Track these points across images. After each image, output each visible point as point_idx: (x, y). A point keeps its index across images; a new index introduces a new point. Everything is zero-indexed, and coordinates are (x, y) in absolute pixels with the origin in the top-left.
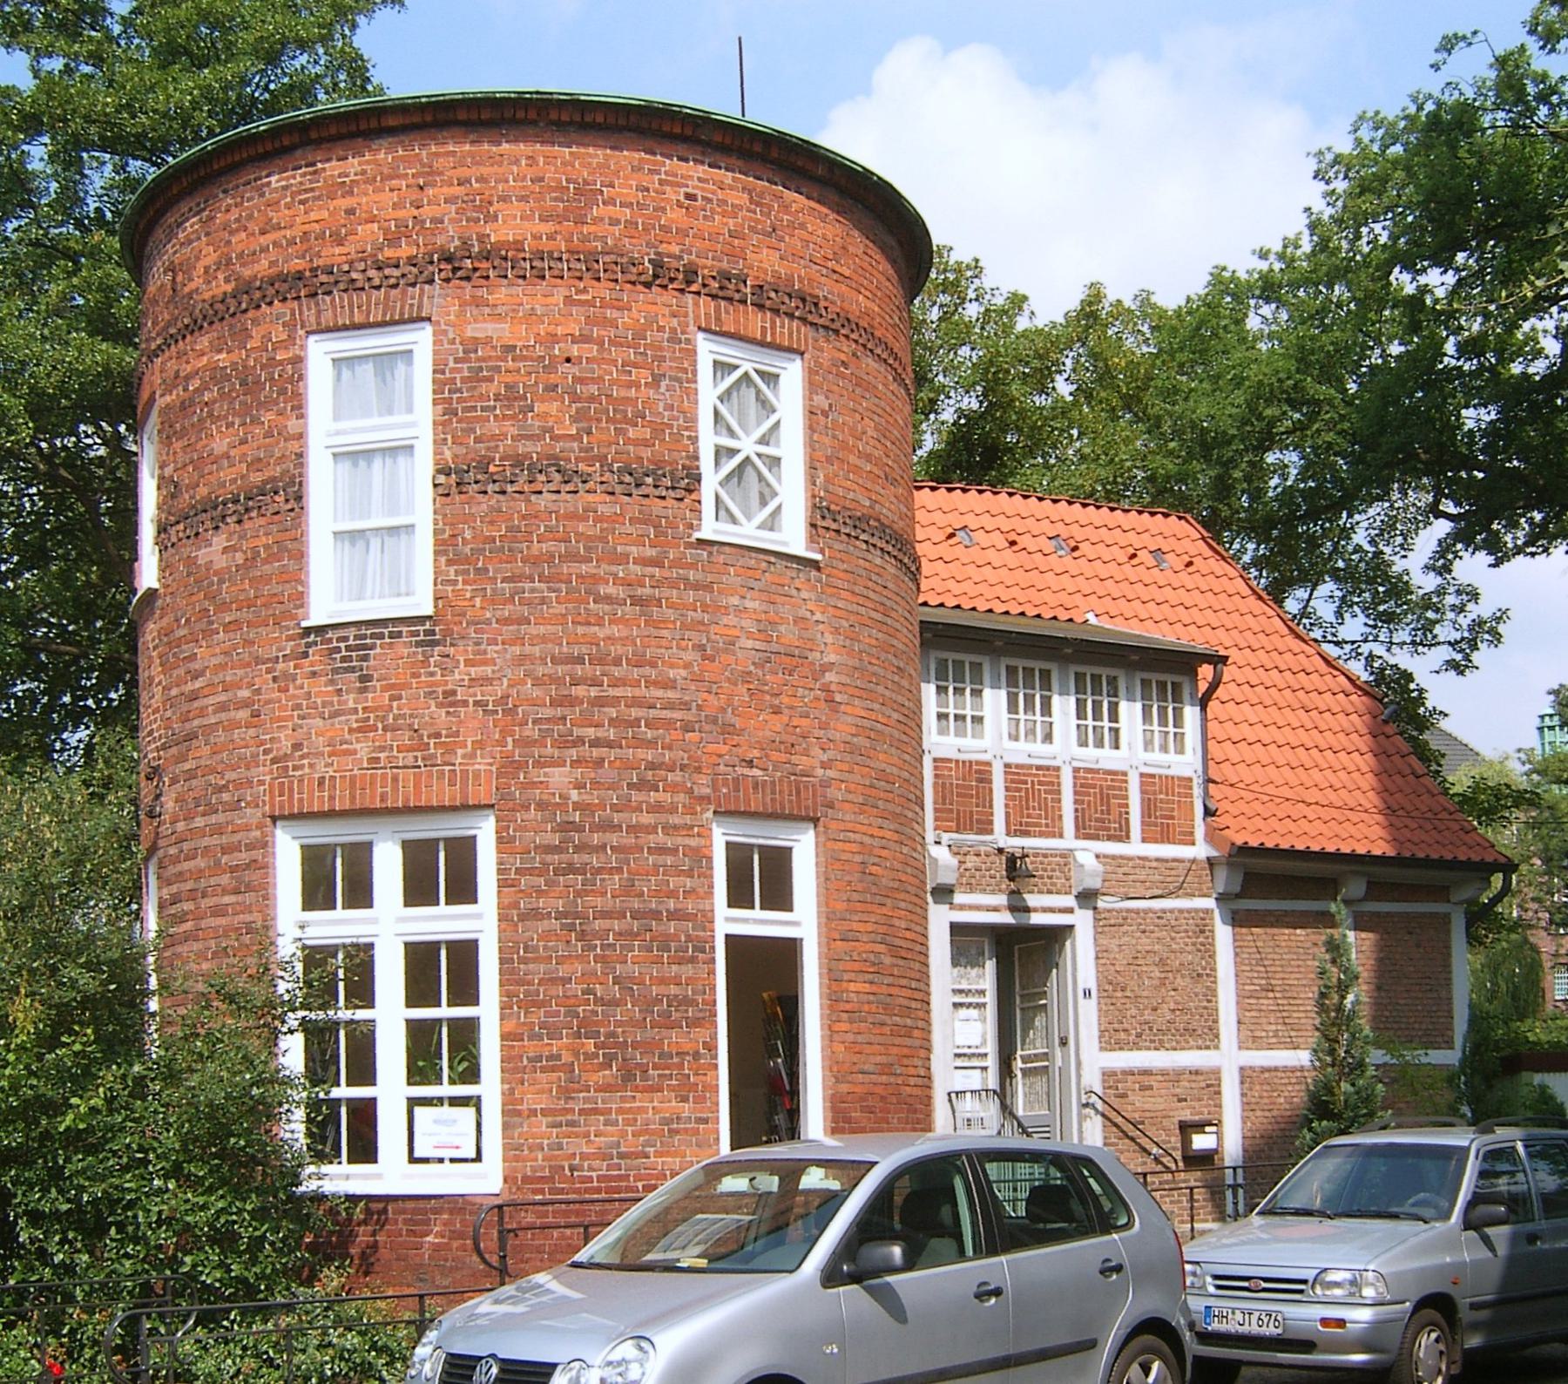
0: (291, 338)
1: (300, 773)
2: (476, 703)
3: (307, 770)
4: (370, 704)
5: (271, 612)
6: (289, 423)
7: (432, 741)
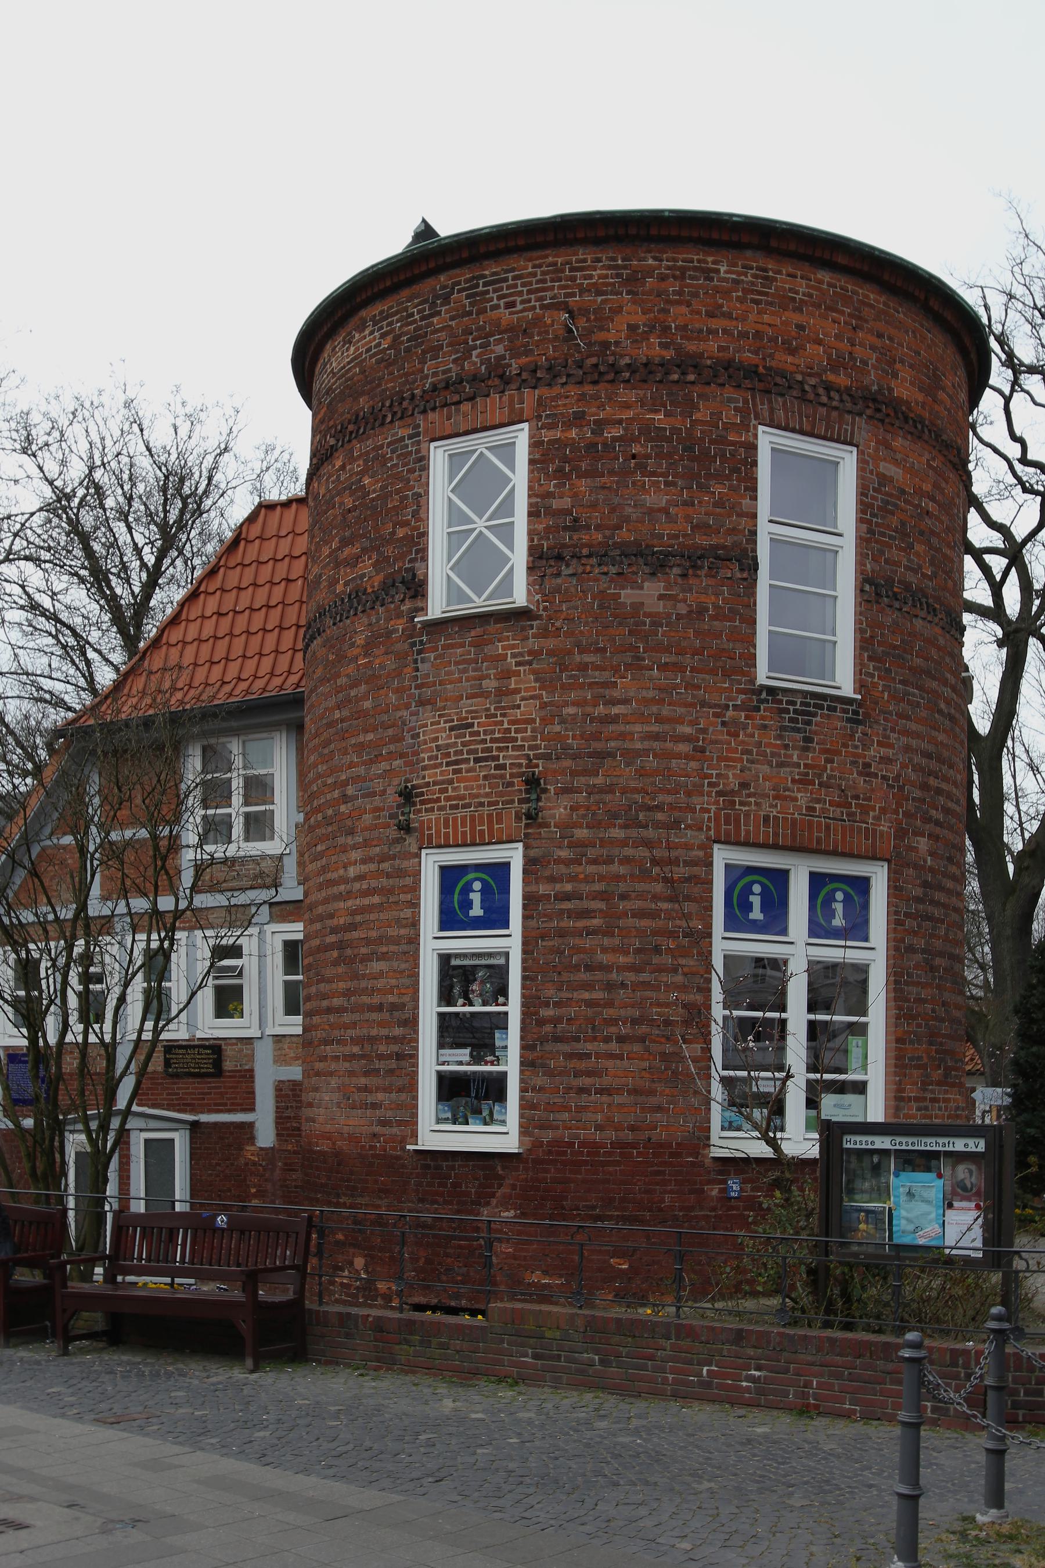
0: (745, 426)
1: (747, 808)
2: (883, 777)
3: (753, 807)
5: (721, 664)
6: (744, 502)
7: (854, 802)
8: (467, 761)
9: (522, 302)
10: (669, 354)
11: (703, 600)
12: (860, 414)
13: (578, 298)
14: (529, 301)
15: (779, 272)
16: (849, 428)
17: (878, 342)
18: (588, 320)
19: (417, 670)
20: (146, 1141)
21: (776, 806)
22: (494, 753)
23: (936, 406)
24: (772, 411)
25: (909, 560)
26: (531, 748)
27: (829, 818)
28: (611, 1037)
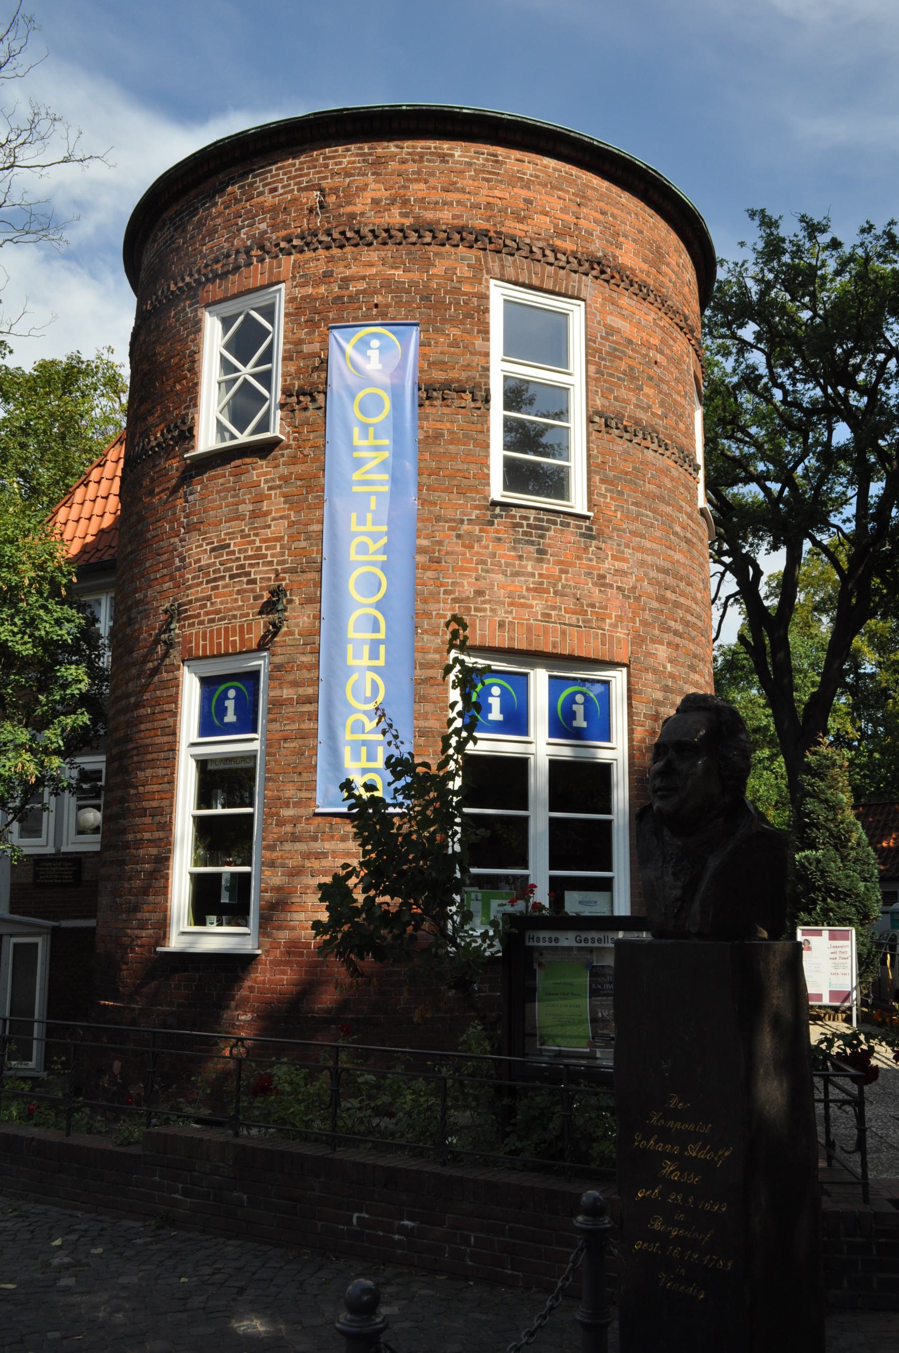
1: (482, 614)
2: (619, 588)
3: (488, 613)
4: (544, 572)
5: (456, 483)
7: (589, 610)
8: (223, 578)
9: (283, 187)
10: (408, 222)
11: (439, 427)
12: (587, 274)
13: (329, 180)
14: (289, 185)
15: (509, 158)
16: (576, 285)
17: (601, 217)
18: (338, 197)
19: (187, 501)
20: (15, 945)
21: (511, 612)
22: (247, 570)
23: (660, 277)
24: (502, 267)
25: (638, 399)
26: (279, 563)
27: (565, 624)
28: (348, 835)
